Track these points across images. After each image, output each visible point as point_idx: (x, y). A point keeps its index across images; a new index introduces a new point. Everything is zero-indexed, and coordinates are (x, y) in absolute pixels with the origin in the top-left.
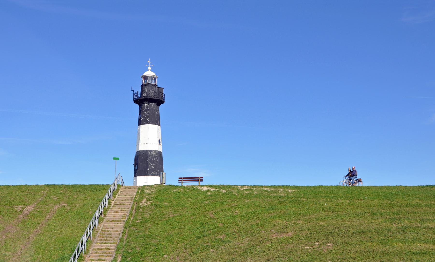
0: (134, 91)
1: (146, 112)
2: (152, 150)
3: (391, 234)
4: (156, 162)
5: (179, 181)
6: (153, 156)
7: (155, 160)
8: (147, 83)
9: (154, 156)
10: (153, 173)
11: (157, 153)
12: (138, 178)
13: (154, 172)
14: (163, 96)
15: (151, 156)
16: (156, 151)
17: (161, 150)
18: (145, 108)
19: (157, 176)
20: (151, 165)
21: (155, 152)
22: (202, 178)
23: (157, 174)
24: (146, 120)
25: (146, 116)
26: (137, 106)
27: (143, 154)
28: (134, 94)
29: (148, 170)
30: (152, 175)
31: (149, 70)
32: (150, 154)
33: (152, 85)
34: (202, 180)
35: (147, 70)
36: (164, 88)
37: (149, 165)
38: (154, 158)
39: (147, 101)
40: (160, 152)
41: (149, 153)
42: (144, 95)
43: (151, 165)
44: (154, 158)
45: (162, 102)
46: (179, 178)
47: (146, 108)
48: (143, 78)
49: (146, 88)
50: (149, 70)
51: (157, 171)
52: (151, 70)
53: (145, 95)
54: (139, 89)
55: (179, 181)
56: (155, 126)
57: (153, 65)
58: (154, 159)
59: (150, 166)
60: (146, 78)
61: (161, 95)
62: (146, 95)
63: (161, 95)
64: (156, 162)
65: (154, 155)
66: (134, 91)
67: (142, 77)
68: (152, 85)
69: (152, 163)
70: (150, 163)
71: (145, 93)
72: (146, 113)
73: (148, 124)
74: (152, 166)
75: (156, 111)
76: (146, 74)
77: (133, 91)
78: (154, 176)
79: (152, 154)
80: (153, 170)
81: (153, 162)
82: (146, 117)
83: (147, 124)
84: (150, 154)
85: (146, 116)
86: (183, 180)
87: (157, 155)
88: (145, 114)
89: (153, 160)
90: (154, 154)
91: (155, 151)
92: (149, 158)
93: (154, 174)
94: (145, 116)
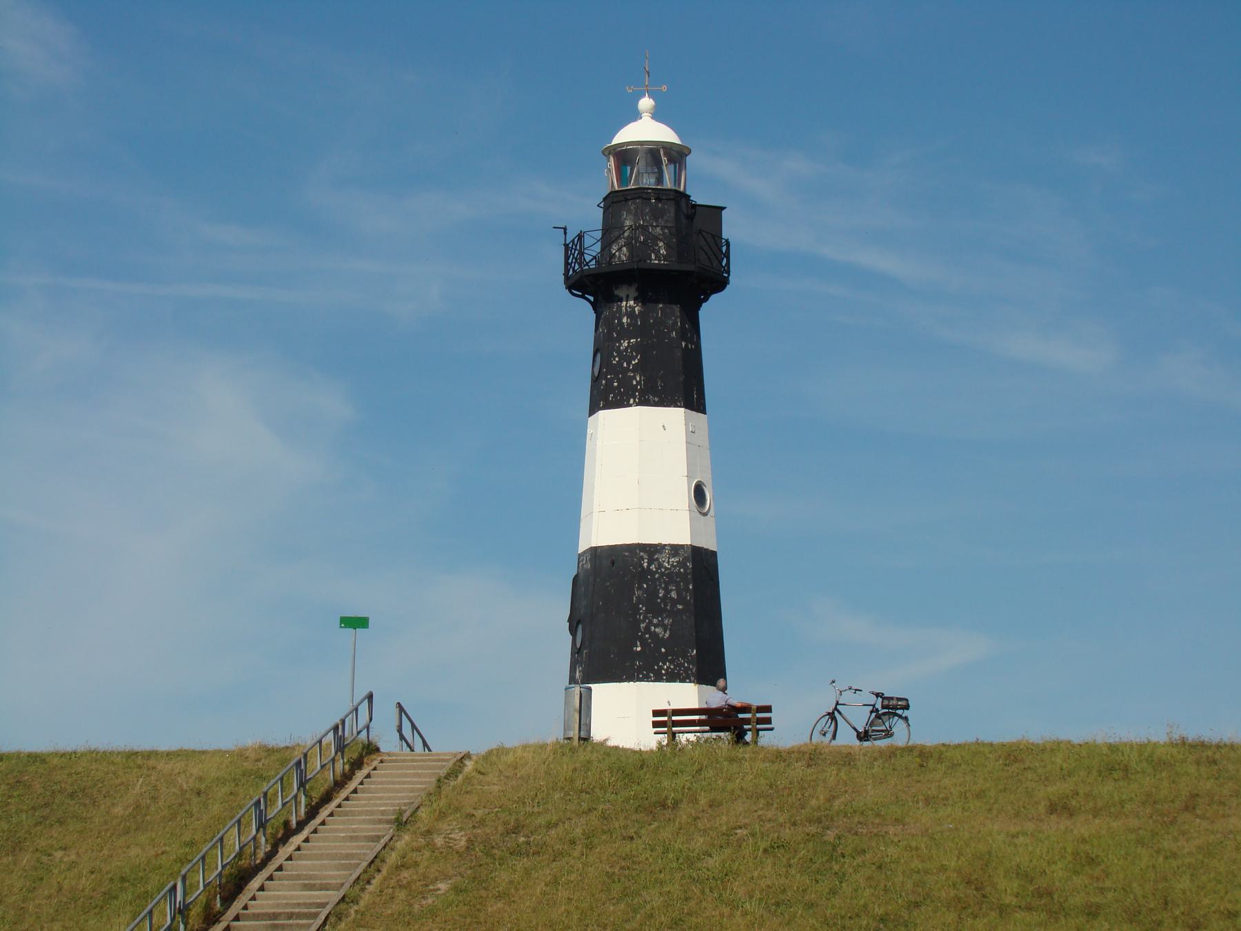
0: (565, 233)
1: (626, 344)
2: (659, 545)
3: (401, 916)
4: (680, 607)
5: (655, 724)
6: (662, 574)
7: (674, 595)
8: (631, 187)
9: (670, 577)
10: (661, 668)
11: (686, 559)
12: (600, 691)
13: (671, 662)
14: (717, 249)
15: (653, 573)
16: (682, 546)
17: (709, 543)
18: (620, 319)
19: (683, 681)
20: (651, 623)
21: (674, 556)
22: (768, 709)
23: (687, 669)
24: (626, 382)
25: (625, 365)
26: (582, 312)
27: (613, 563)
28: (566, 245)
29: (639, 649)
30: (658, 679)
31: (646, 118)
32: (645, 565)
33: (658, 199)
34: (768, 721)
35: (635, 116)
36: (724, 208)
37: (644, 621)
38: (667, 584)
39: (630, 284)
40: (706, 550)
41: (642, 558)
42: (621, 254)
43: (655, 621)
44: (667, 584)
45: (720, 284)
46: (656, 713)
47: (625, 320)
48: (612, 159)
49: (629, 212)
50: (646, 118)
51: (685, 656)
52: (657, 115)
53: (620, 249)
54: (595, 218)
55: (654, 727)
56: (675, 417)
57: (664, 88)
58: (667, 591)
59: (647, 629)
60: (624, 156)
61: (706, 248)
62: (624, 249)
63: (706, 248)
64: (680, 607)
65: (666, 569)
66: (565, 233)
67: (606, 153)
68: (661, 194)
69: (654, 610)
70: (647, 611)
71: (622, 242)
72: (627, 348)
73: (638, 405)
74: (656, 626)
75: (683, 335)
76: (629, 134)
77: (565, 229)
78: (668, 681)
79: (660, 566)
80: (663, 650)
81: (666, 605)
82: (628, 369)
83: (631, 406)
84: (649, 565)
85: (625, 365)
86: (749, 712)
87: (686, 567)
88: (618, 351)
89: (665, 595)
90: (668, 562)
91: (675, 549)
92: (640, 588)
93: (666, 670)
94: (620, 364)
